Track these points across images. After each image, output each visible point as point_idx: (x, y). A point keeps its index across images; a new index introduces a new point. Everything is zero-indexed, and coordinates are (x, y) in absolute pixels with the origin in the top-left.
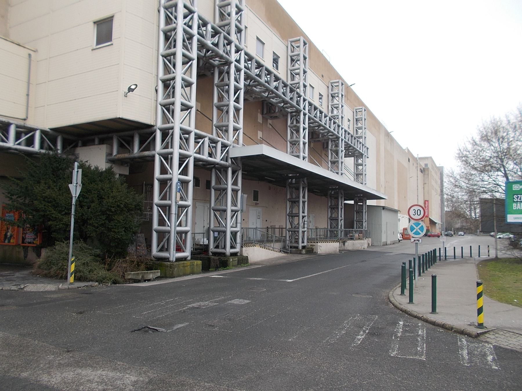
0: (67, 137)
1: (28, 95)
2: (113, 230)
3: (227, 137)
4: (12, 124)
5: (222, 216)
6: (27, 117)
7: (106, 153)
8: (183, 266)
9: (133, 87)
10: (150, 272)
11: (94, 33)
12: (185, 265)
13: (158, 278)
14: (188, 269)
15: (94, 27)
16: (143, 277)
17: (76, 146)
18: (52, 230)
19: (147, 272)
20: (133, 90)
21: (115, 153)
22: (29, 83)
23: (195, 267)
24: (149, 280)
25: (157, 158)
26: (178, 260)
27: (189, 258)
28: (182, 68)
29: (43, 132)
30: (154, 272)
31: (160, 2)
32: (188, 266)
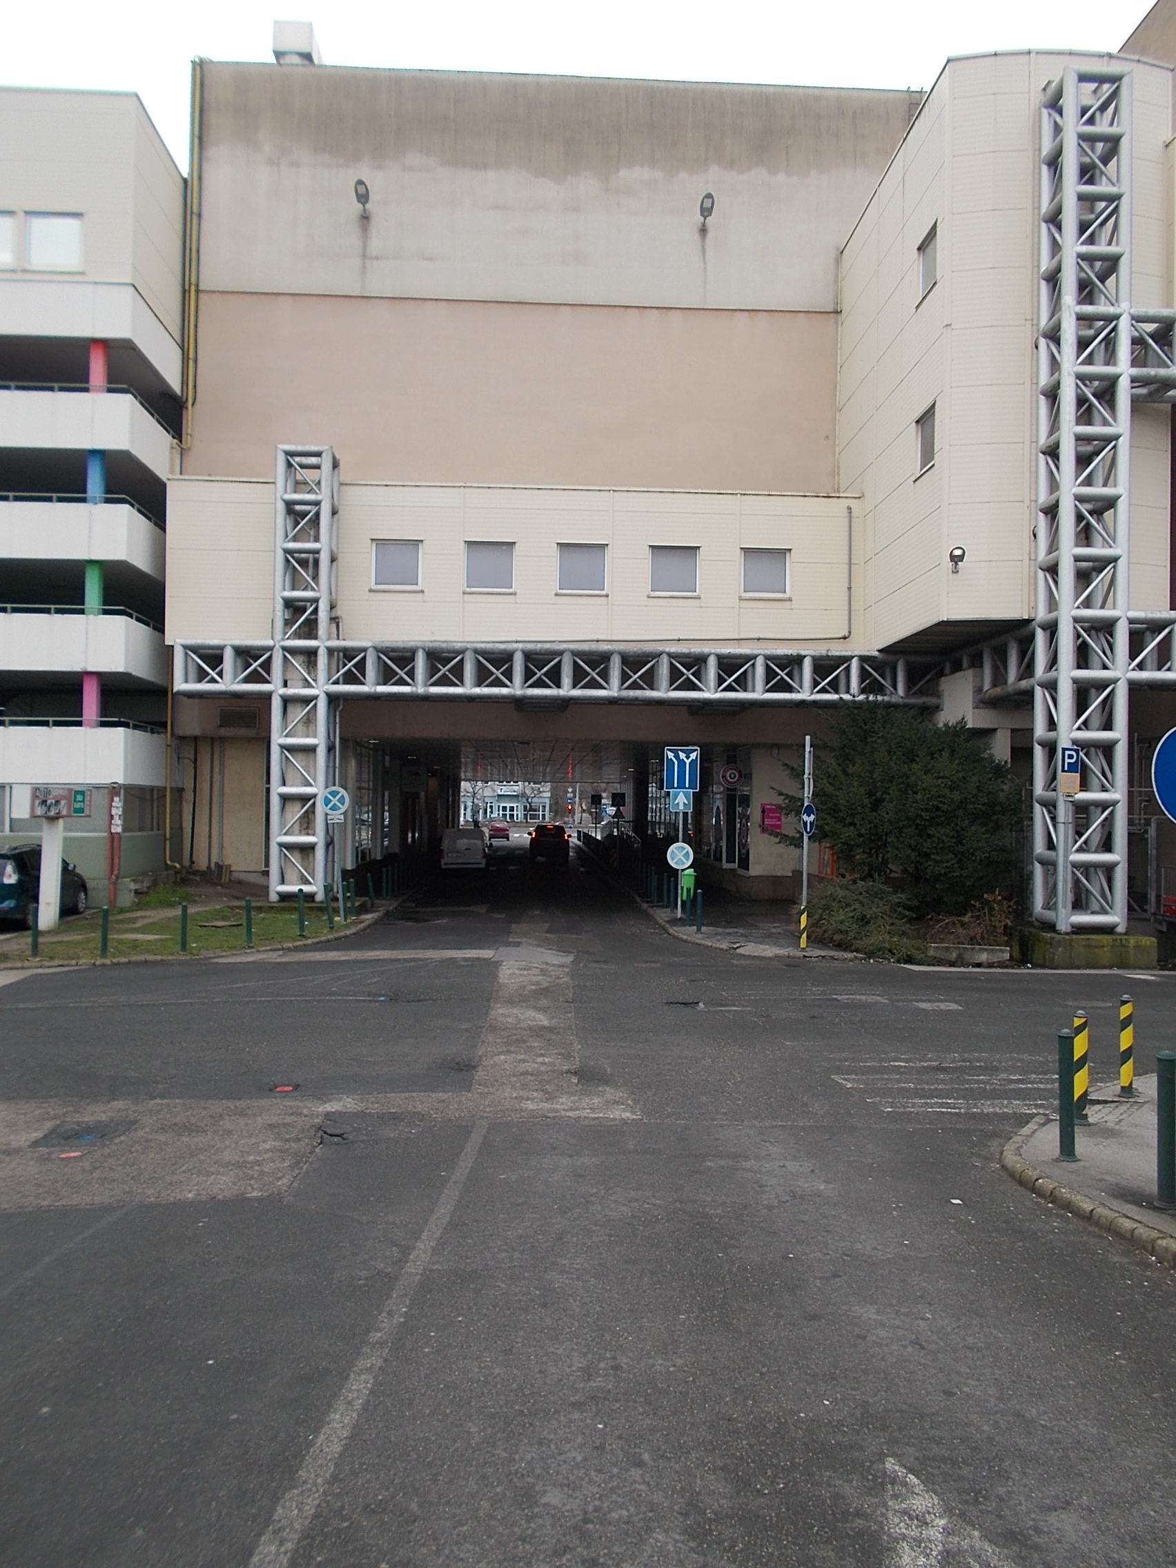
0: (913, 658)
1: (850, 588)
2: (933, 857)
3: (889, 681)
4: (805, 656)
5: (221, 816)
6: (850, 632)
7: (974, 687)
8: (1085, 946)
9: (958, 552)
10: (980, 949)
11: (917, 444)
12: (1093, 943)
13: (1001, 965)
14: (1106, 955)
15: (917, 432)
16: (960, 956)
17: (941, 674)
18: (574, 841)
19: (973, 949)
20: (961, 558)
21: (987, 686)
22: (850, 564)
23: (1132, 952)
24: (979, 965)
25: (1038, 691)
26: (1079, 929)
27: (1120, 929)
28: (1076, 471)
29: (863, 659)
30: (992, 950)
31: (3, 941)
32: (1103, 946)
